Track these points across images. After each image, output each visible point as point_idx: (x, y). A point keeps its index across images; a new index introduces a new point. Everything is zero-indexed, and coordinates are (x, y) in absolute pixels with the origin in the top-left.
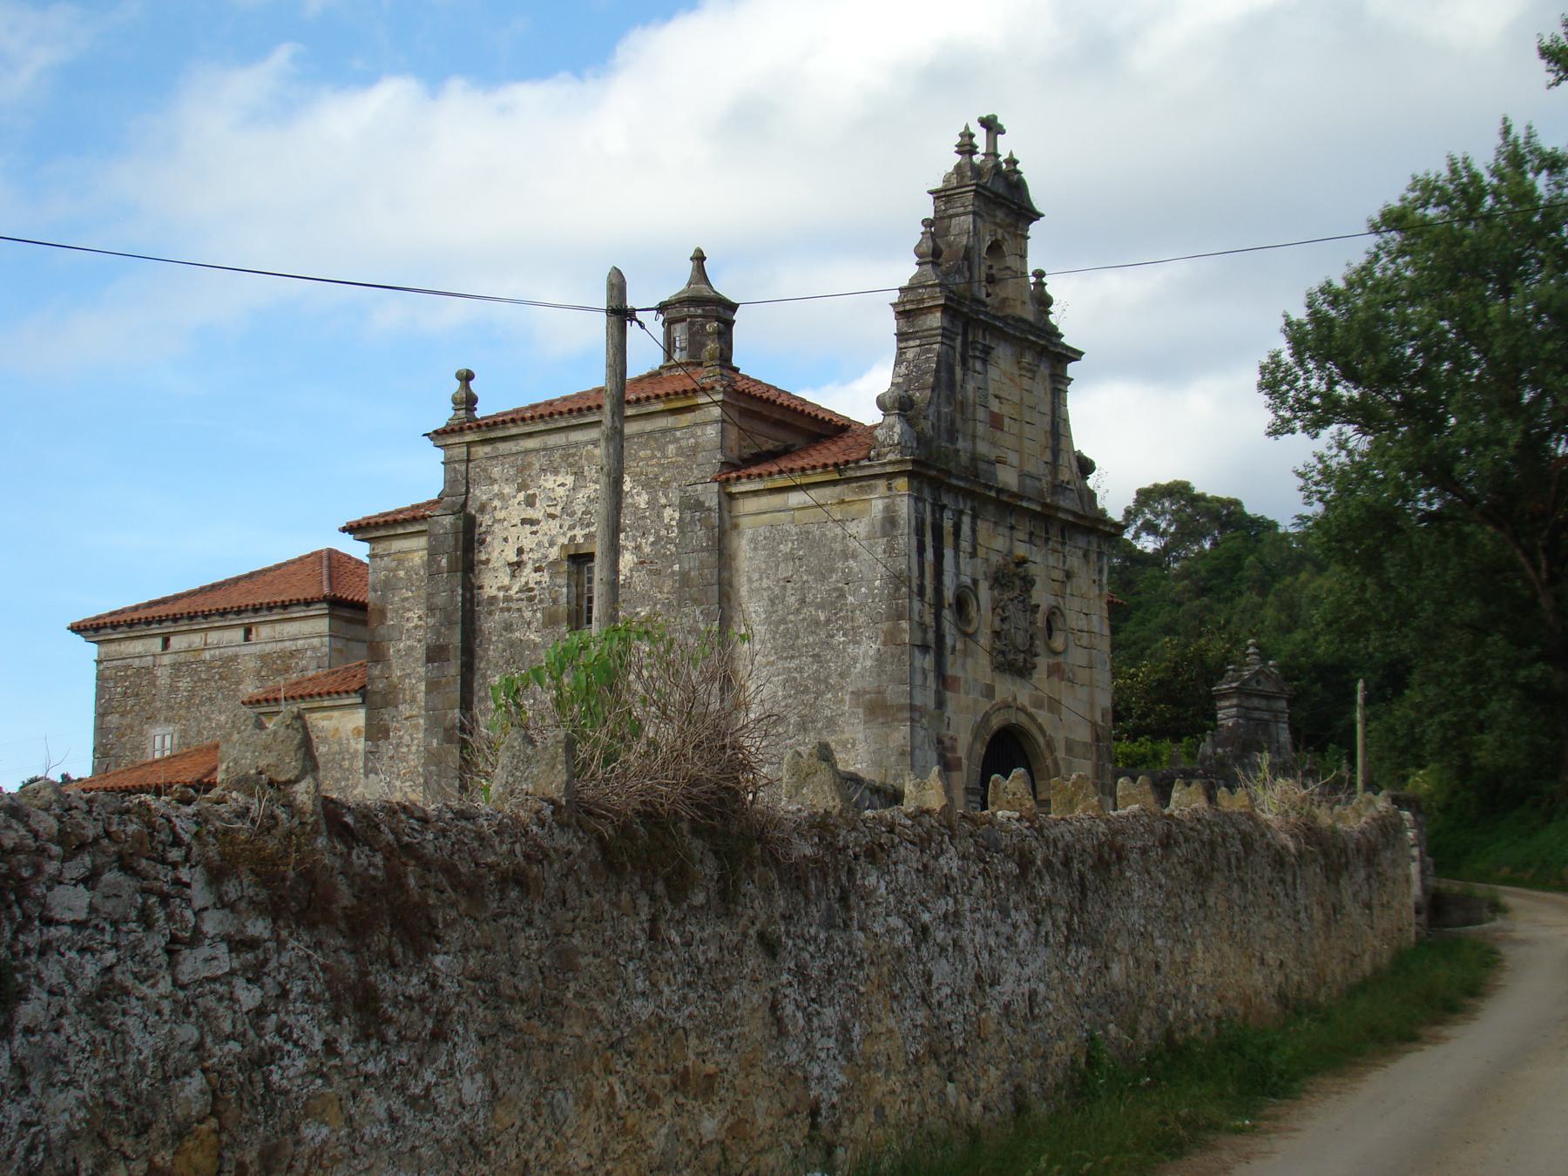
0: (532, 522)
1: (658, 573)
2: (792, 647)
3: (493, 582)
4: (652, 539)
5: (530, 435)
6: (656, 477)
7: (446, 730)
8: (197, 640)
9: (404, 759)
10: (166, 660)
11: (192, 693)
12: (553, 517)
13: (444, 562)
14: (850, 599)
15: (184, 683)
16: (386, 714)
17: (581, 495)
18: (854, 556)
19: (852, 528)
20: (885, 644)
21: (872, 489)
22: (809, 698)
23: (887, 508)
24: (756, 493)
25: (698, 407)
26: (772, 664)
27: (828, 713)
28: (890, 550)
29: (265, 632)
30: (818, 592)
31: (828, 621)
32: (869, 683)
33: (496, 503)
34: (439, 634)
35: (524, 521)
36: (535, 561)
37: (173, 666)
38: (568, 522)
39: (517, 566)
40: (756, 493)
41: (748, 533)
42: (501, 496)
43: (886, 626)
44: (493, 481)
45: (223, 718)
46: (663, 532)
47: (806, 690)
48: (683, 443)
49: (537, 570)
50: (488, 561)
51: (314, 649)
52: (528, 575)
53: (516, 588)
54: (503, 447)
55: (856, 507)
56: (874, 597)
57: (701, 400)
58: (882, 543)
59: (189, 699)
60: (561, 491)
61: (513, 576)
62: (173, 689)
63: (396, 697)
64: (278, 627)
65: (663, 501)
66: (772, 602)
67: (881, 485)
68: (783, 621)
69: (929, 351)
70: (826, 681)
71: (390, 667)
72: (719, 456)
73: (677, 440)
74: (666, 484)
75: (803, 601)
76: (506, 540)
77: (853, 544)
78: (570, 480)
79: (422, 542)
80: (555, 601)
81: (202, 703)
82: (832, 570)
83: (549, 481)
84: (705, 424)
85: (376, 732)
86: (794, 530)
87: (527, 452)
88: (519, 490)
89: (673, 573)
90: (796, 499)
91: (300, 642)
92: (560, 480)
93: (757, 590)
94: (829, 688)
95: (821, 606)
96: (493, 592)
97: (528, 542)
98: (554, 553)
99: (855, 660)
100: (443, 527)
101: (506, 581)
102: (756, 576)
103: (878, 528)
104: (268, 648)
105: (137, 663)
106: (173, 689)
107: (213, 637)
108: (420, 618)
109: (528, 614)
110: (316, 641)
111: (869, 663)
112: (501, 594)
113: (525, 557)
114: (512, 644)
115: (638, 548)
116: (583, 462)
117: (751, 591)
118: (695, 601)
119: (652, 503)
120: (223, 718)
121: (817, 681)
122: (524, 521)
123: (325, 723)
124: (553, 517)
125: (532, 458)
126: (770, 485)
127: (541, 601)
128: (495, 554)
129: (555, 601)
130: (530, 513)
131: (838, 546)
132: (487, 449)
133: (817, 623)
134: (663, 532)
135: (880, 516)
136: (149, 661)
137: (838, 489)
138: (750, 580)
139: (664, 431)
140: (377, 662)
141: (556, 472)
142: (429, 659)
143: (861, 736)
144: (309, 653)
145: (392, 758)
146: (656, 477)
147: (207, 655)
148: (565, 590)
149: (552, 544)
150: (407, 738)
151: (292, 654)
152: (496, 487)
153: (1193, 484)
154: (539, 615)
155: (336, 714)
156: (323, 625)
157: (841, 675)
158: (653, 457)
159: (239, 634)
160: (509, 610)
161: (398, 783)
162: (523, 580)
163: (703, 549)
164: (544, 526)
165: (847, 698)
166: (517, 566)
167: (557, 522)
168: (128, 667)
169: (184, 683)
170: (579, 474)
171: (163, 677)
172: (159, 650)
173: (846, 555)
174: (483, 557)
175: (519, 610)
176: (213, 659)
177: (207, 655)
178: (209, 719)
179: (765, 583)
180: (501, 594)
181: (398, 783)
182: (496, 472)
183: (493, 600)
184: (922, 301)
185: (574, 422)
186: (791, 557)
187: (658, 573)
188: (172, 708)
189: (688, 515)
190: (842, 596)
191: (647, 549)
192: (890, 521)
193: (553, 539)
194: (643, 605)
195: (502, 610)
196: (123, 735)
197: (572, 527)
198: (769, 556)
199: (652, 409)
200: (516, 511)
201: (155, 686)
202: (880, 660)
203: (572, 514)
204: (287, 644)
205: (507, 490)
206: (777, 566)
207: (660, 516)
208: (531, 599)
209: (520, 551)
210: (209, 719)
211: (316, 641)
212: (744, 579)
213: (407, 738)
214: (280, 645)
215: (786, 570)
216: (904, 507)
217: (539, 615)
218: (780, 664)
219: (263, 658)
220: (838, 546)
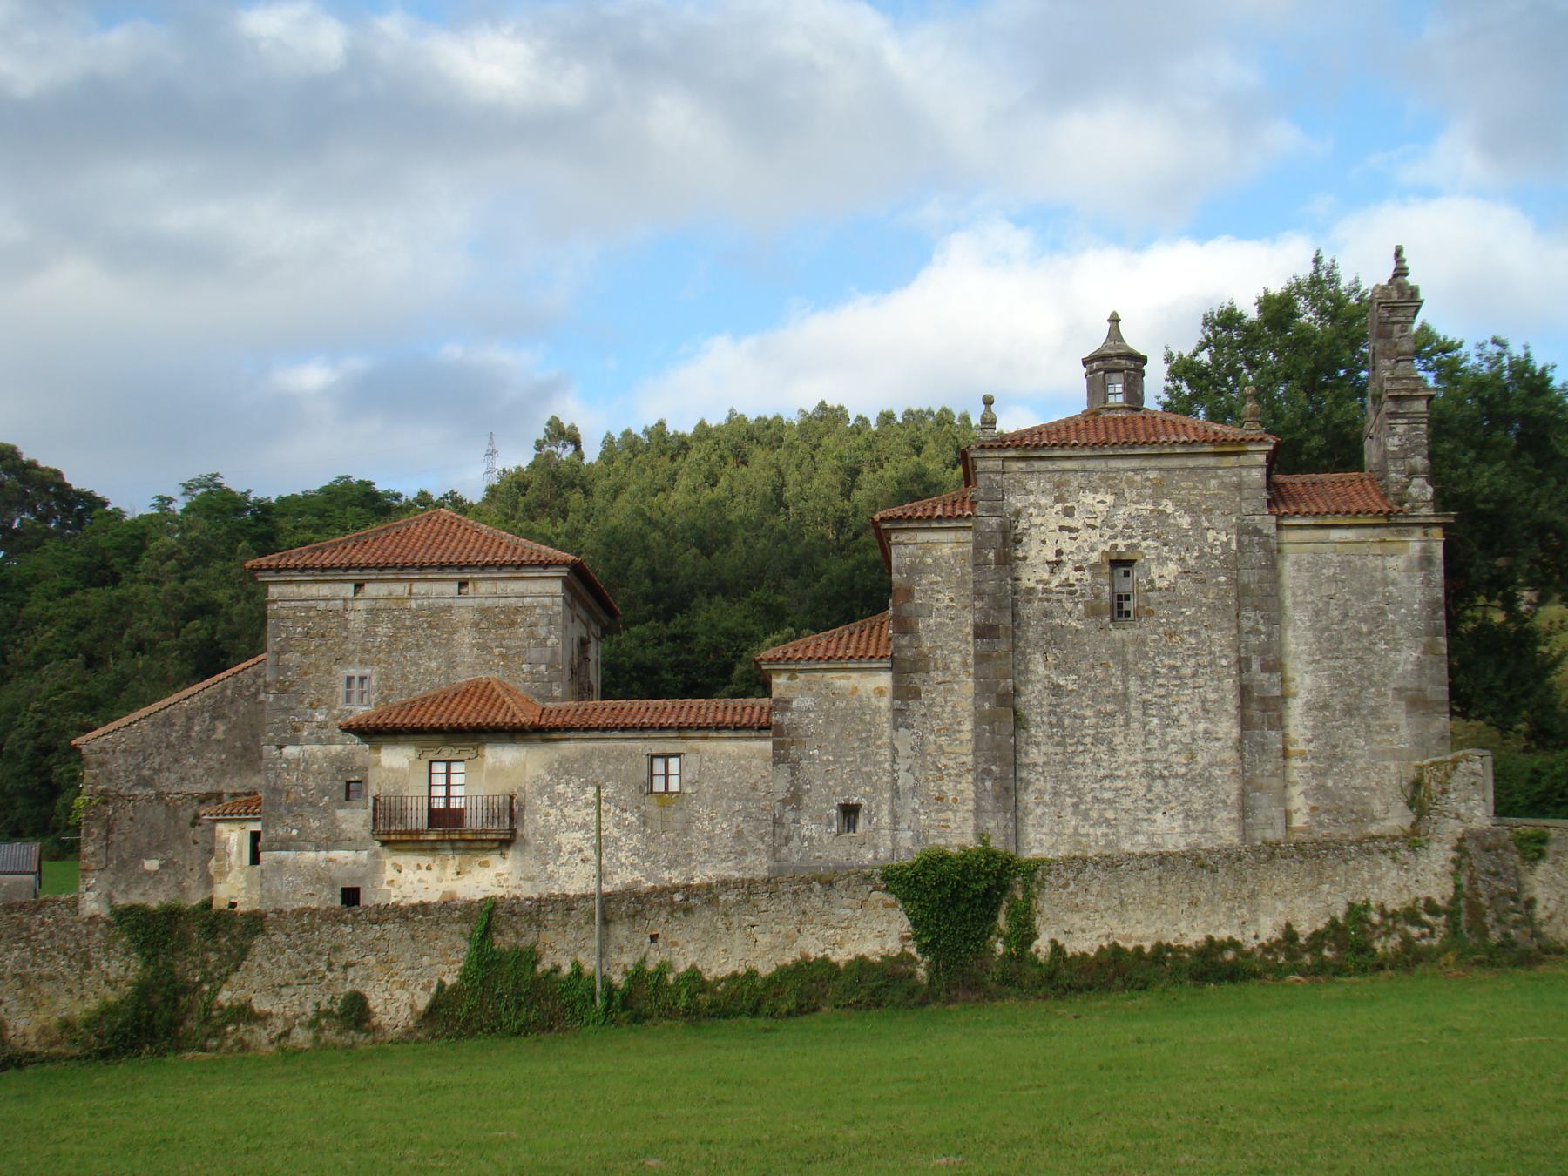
0: (1070, 530)
1: (1203, 582)
2: (1337, 650)
3: (1032, 575)
4: (1196, 554)
5: (1069, 458)
6: (1198, 504)
7: (999, 696)
8: (400, 589)
9: (937, 717)
10: (361, 605)
11: (394, 638)
12: (1094, 527)
13: (991, 556)
14: (1391, 616)
15: (384, 629)
16: (917, 679)
17: (1122, 513)
18: (1394, 583)
19: (1391, 562)
20: (1424, 653)
21: (1409, 534)
22: (1355, 690)
23: (1424, 550)
24: (1300, 527)
25: (1245, 453)
26: (1318, 662)
27: (1372, 703)
28: (1427, 582)
29: (484, 587)
30: (1361, 608)
31: (1370, 633)
32: (1411, 682)
33: (1031, 510)
34: (988, 617)
35: (1062, 528)
36: (1075, 562)
37: (370, 611)
38: (1108, 533)
39: (1055, 565)
40: (1300, 527)
41: (1292, 557)
42: (1037, 505)
43: (1425, 639)
44: (1029, 492)
45: (434, 664)
46: (1207, 549)
47: (1351, 685)
48: (1227, 480)
49: (1077, 569)
50: (1025, 558)
51: (544, 607)
52: (1068, 572)
53: (1055, 582)
54: (1037, 465)
55: (1395, 546)
56: (1413, 616)
57: (1250, 448)
58: (1419, 577)
59: (389, 645)
60: (1101, 507)
61: (1052, 572)
62: (369, 633)
63: (927, 665)
64: (500, 585)
65: (1206, 524)
66: (1316, 613)
67: (1418, 532)
68: (1327, 629)
69: (1416, 429)
70: (1369, 678)
71: (919, 639)
72: (1265, 494)
73: (1217, 477)
74: (1208, 511)
75: (1346, 615)
76: (1044, 542)
77: (1393, 574)
78: (1110, 499)
79: (969, 536)
80: (1097, 597)
81: (407, 649)
82: (1373, 593)
83: (1088, 498)
84: (1251, 467)
85: (904, 692)
86: (1336, 559)
87: (1065, 471)
88: (1057, 501)
89: (1218, 583)
90: (1335, 535)
91: (527, 601)
92: (1100, 497)
93: (1302, 603)
94: (1373, 684)
95: (1364, 620)
96: (1032, 584)
97: (1067, 546)
98: (1095, 557)
99: (1397, 664)
100: (989, 526)
101: (1046, 576)
102: (1300, 592)
103: (1416, 564)
104: (489, 603)
105: (322, 605)
106: (369, 633)
107: (419, 588)
108: (951, 600)
109: (1069, 606)
110: (547, 601)
111: (1409, 667)
112: (1040, 587)
113: (1064, 558)
114: (1053, 629)
115: (1182, 560)
116: (1123, 485)
117: (1295, 603)
118: (1256, 608)
119: (1195, 524)
120: (434, 664)
121: (1361, 677)
122: (1062, 528)
123: (843, 682)
124: (1094, 527)
125: (1071, 477)
126: (1320, 522)
127: (1082, 595)
128: (1033, 553)
129: (1097, 597)
130: (1068, 522)
131: (1378, 575)
132: (1022, 465)
133: (1360, 633)
134: (1207, 549)
135: (1417, 555)
136: (339, 604)
137: (1377, 531)
138: (1294, 595)
139: (1206, 468)
140: (906, 633)
141: (1096, 491)
142: (977, 635)
143: (1403, 723)
144: (538, 611)
145: (924, 715)
146: (1198, 504)
147: (413, 604)
148: (1107, 588)
149: (1092, 549)
150: (940, 700)
151: (517, 610)
152: (1032, 498)
153: (20, 449)
154: (1080, 606)
155: (855, 675)
156: (557, 587)
157: (1384, 675)
158: (1195, 488)
159: (453, 588)
160: (1048, 600)
161: (932, 737)
162: (1063, 577)
163: (1262, 567)
164: (1084, 534)
165: (1390, 693)
166: (1055, 565)
167: (1098, 532)
168: (310, 609)
169: (384, 629)
170: (1119, 495)
171: (357, 621)
172: (351, 594)
173: (1386, 582)
174: (1020, 554)
175: (1059, 601)
176: (420, 608)
177: (413, 604)
178: (416, 664)
179: (1309, 598)
180: (1040, 587)
181: (932, 737)
182: (1032, 485)
183: (1030, 591)
184: (1416, 390)
185: (1121, 452)
186: (1333, 579)
187: (1203, 582)
188: (370, 652)
189: (1246, 539)
190: (1383, 613)
191: (1192, 562)
192: (1426, 560)
193: (1094, 545)
194: (1187, 606)
195: (1041, 600)
196: (306, 674)
197: (1113, 537)
198: (1313, 577)
199: (1202, 450)
200: (1054, 517)
201: (346, 628)
202: (1420, 665)
203: (1113, 527)
204: (512, 600)
205: (1043, 501)
206: (1321, 585)
207: (1203, 537)
208: (1071, 593)
209: (1059, 552)
210: (416, 664)
211: (547, 601)
212: (1288, 593)
213: (940, 700)
214: (502, 602)
215: (1325, 591)
216: (1438, 551)
217: (1080, 606)
218: (1325, 663)
219: (483, 611)
220: (1378, 575)
